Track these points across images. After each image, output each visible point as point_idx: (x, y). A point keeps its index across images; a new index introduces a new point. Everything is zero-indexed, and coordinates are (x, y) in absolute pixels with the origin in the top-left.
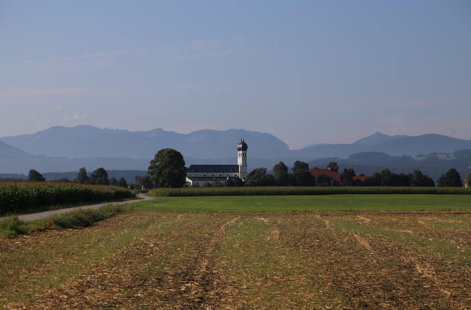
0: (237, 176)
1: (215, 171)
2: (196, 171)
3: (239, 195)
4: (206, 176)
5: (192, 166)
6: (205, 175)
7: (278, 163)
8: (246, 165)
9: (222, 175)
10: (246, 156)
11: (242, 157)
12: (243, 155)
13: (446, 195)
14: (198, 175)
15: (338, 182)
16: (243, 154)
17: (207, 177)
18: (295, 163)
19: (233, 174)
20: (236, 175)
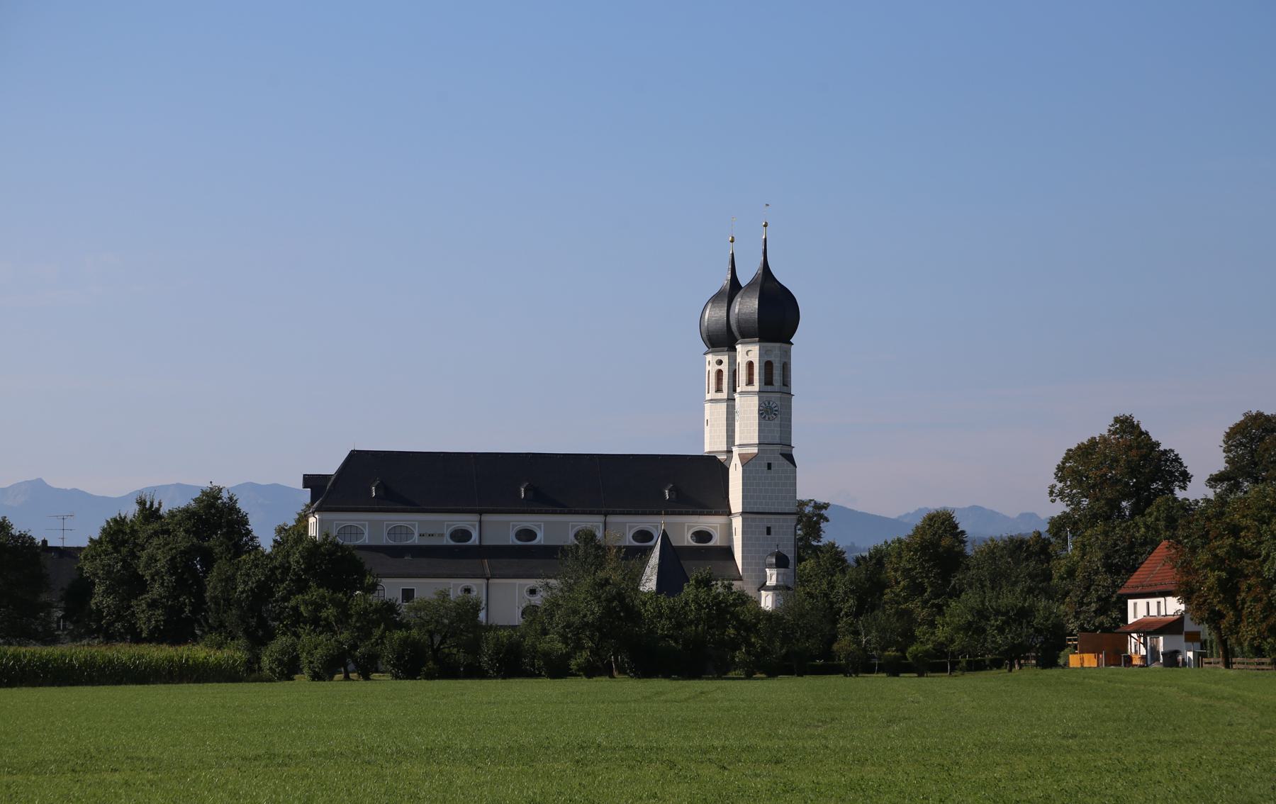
0: (716, 541)
1: (543, 501)
2: (393, 500)
3: (119, 682)
4: (475, 540)
5: (356, 458)
6: (462, 535)
7: (1100, 427)
8: (790, 458)
9: (475, 535)
10: (786, 382)
11: (756, 387)
12: (768, 380)
13: (737, 681)
14: (359, 533)
15: (193, 545)
16: (768, 367)
17: (483, 552)
18: (1230, 435)
19: (684, 529)
20: (703, 536)
